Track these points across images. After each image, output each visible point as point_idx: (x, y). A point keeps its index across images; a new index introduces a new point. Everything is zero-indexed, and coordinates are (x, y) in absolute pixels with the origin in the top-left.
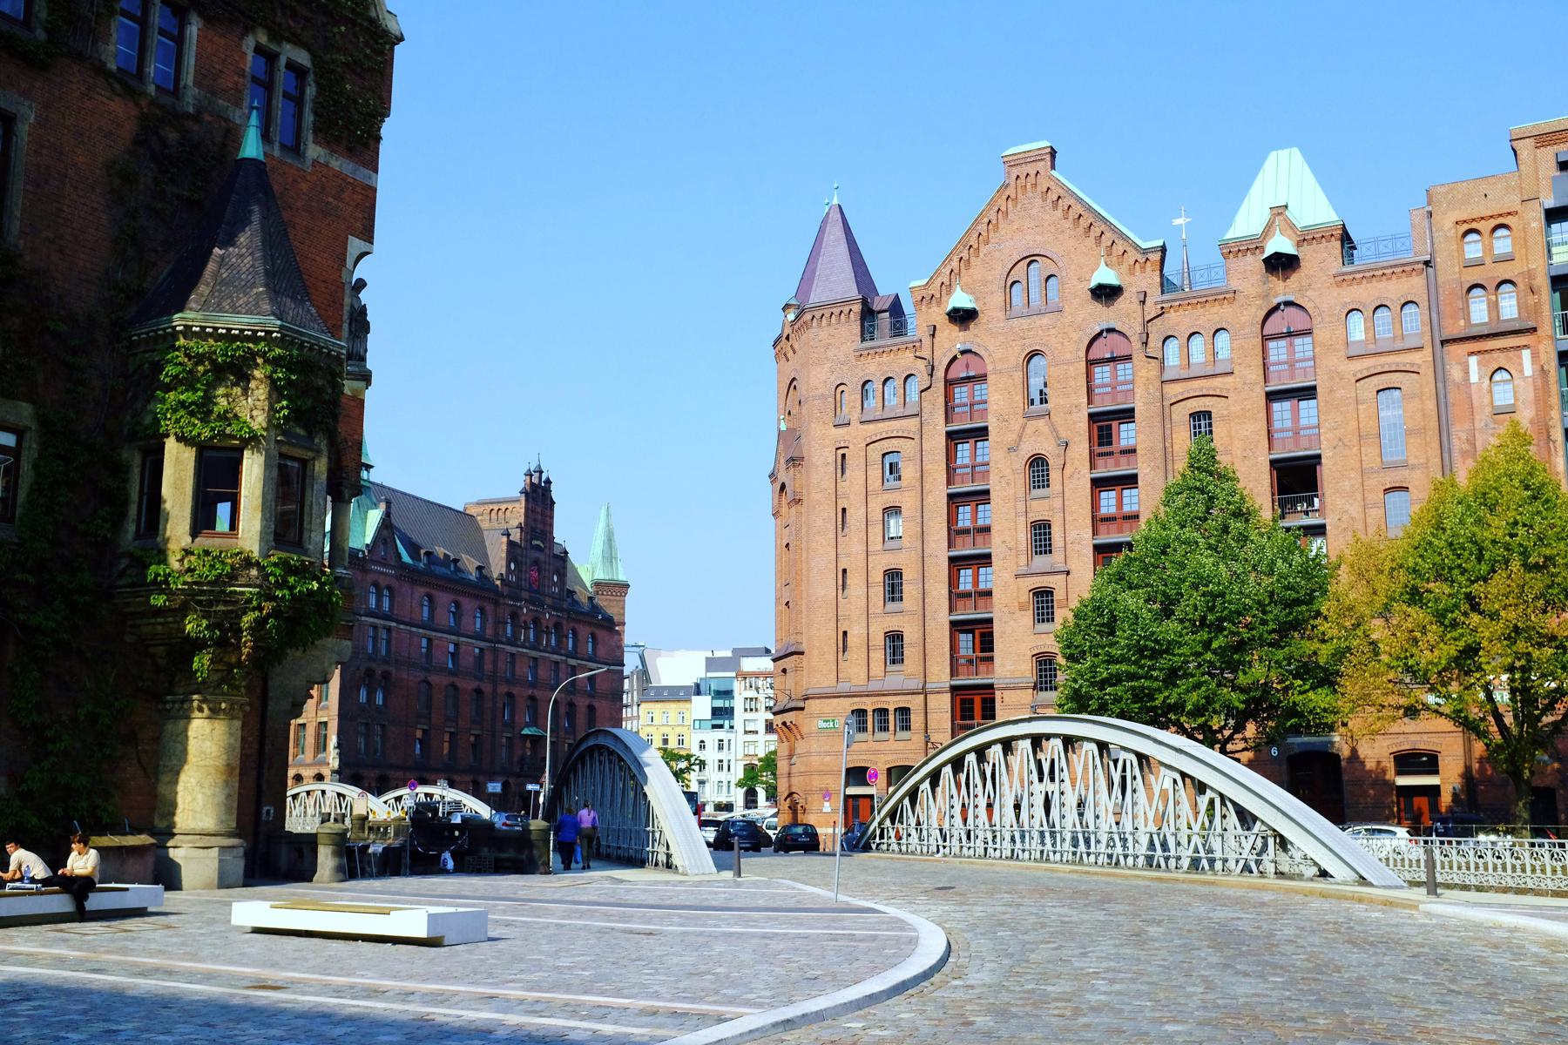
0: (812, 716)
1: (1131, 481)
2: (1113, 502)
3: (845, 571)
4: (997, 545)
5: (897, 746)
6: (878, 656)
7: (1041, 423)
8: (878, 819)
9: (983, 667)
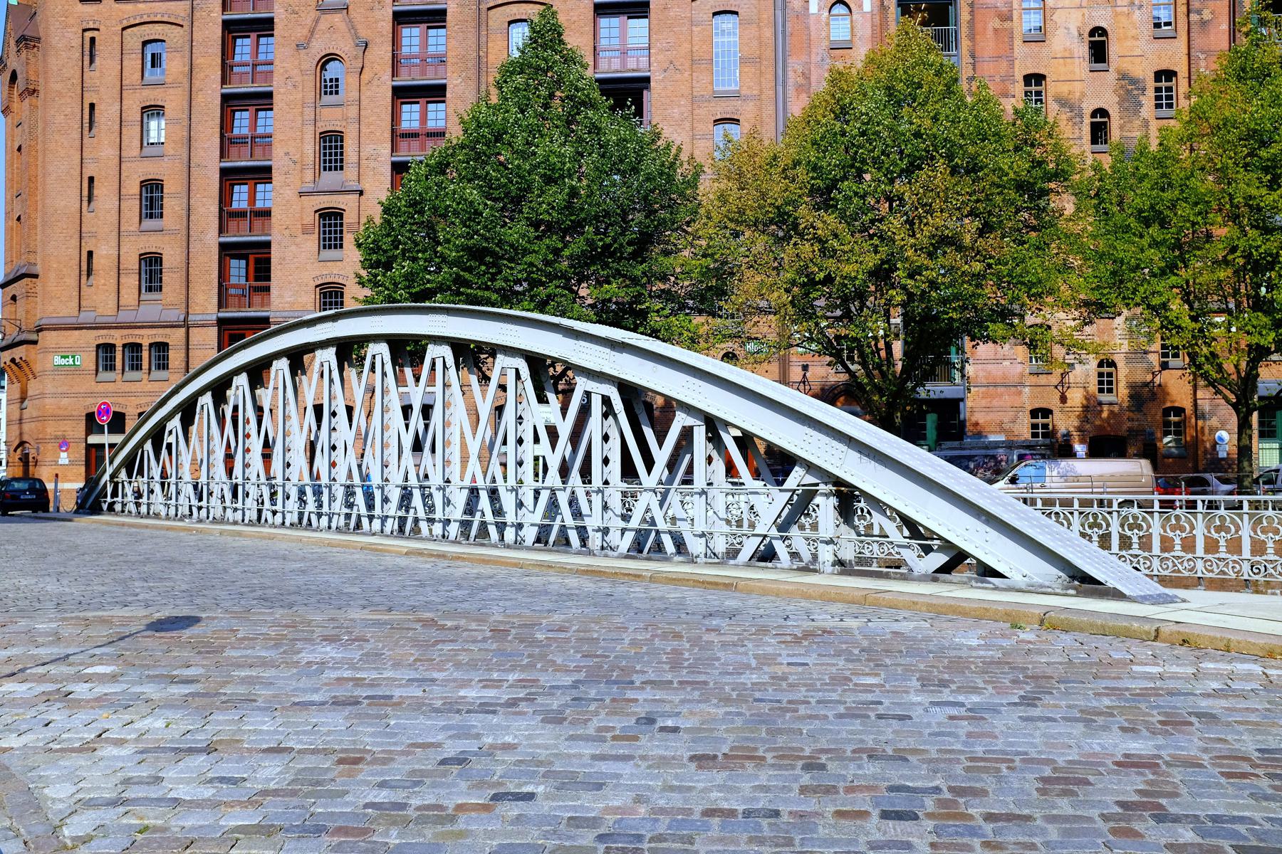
0: (46, 351)
1: (436, 92)
2: (416, 116)
3: (91, 179)
4: (279, 161)
6: (131, 282)
7: (337, 18)
8: (110, 470)
9: (257, 299)
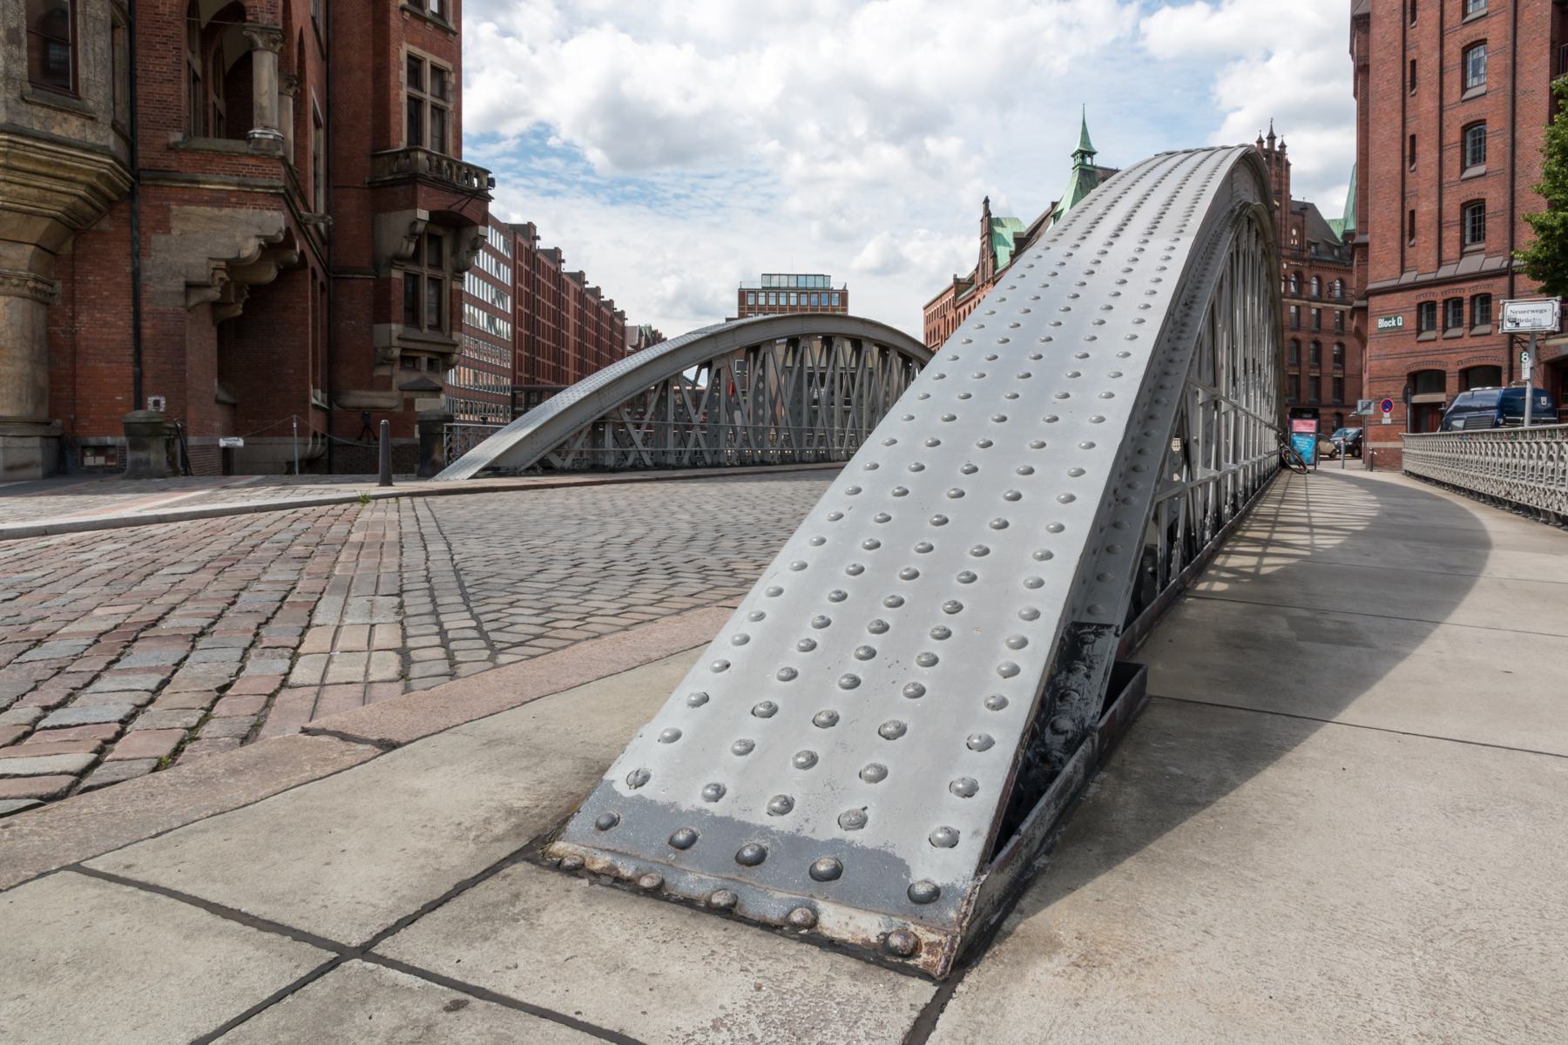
5: (1471, 342)
